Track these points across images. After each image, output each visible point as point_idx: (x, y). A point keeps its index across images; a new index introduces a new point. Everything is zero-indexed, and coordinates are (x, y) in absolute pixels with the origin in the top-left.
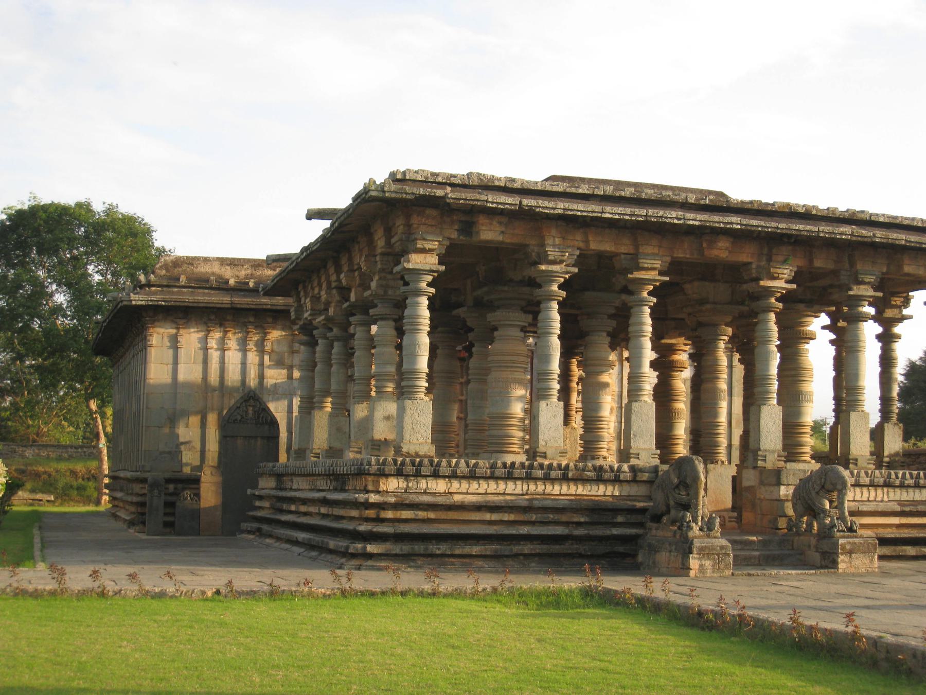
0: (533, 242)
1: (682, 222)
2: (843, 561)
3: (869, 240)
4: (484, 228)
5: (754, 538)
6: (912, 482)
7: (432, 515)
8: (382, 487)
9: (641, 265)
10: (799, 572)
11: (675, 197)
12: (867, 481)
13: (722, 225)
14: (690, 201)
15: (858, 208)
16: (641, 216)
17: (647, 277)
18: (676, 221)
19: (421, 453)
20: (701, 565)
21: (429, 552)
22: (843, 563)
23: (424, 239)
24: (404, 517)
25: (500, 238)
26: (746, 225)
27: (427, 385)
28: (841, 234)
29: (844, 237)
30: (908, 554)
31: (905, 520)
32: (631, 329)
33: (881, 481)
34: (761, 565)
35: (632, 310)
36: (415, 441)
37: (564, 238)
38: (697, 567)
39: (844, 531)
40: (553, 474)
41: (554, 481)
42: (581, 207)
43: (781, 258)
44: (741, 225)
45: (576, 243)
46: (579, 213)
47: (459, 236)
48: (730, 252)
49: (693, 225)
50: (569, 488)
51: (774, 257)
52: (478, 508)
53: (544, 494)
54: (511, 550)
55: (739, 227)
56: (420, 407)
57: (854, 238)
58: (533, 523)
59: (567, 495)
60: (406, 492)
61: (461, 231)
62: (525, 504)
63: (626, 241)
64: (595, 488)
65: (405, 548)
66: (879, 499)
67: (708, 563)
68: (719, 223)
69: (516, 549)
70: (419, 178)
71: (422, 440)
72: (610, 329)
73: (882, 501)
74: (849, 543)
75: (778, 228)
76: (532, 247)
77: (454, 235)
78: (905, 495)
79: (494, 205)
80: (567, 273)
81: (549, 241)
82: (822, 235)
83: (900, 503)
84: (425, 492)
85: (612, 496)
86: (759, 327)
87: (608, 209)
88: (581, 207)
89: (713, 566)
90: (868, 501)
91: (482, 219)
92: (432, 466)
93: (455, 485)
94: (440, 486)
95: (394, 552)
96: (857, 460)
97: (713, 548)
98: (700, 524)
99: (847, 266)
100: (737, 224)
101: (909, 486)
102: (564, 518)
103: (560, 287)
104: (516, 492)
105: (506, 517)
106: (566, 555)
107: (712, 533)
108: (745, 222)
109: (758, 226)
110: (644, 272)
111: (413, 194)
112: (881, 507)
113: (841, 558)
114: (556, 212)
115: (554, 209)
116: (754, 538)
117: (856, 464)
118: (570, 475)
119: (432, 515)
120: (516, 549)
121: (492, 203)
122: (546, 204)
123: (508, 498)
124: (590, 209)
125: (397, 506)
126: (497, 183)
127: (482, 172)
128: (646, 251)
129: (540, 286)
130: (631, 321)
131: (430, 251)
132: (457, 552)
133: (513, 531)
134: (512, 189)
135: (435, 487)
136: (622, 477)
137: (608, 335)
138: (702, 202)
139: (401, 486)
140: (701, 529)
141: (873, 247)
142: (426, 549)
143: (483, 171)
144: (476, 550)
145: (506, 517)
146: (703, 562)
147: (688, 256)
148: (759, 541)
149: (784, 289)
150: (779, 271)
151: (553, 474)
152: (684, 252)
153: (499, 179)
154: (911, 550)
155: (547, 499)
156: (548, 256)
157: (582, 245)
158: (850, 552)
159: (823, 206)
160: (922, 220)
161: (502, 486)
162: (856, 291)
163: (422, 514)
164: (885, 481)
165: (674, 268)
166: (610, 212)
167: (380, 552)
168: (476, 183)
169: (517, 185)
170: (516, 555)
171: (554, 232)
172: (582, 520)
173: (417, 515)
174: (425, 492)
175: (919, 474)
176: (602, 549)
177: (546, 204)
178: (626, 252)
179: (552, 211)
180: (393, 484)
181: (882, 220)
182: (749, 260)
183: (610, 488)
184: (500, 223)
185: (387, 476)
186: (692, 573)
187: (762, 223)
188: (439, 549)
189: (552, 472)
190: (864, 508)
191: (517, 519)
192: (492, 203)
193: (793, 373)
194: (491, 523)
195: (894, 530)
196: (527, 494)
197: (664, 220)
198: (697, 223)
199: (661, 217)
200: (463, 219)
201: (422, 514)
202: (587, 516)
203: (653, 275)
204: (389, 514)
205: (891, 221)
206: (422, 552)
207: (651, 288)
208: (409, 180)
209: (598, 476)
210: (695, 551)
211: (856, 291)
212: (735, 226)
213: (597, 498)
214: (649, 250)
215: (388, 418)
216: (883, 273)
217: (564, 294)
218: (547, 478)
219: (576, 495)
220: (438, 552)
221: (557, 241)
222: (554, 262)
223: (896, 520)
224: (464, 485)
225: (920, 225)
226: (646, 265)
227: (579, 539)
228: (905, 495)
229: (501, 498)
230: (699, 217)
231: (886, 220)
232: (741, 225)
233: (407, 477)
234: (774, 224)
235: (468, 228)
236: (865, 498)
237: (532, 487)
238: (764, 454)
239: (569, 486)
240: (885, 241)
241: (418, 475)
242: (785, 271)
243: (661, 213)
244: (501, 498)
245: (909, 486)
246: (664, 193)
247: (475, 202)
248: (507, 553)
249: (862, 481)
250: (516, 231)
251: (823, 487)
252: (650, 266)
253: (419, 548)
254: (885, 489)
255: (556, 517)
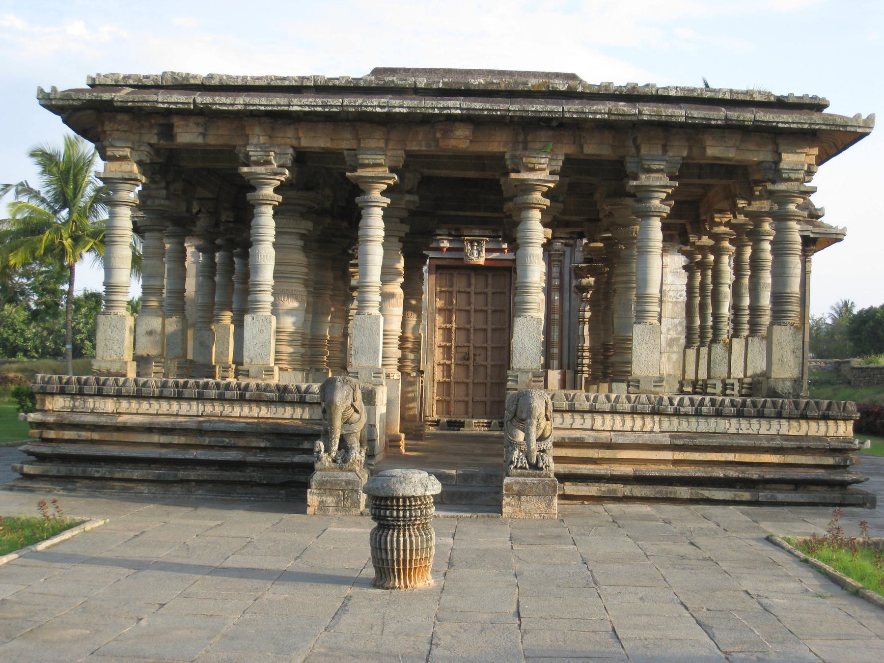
0: (239, 142)
1: (386, 110)
2: (509, 504)
3: (634, 118)
4: (179, 130)
5: (454, 472)
6: (690, 409)
7: (96, 436)
8: (49, 406)
9: (361, 161)
10: (449, 514)
11: (400, 82)
12: (627, 407)
13: (437, 111)
14: (419, 85)
15: (742, 87)
16: (336, 106)
17: (369, 174)
18: (379, 110)
19: (112, 371)
20: (321, 502)
21: (88, 475)
22: (509, 505)
23: (113, 146)
24: (66, 437)
25: (200, 140)
26: (468, 109)
27: (272, 299)
28: (595, 113)
29: (598, 116)
30: (678, 496)
31: (679, 456)
32: (360, 233)
33: (648, 408)
34: (444, 503)
35: (363, 212)
36: (108, 358)
37: (270, 137)
38: (316, 503)
39: (525, 468)
40: (228, 394)
41: (231, 401)
42: (264, 101)
43: (538, 145)
44: (461, 109)
45: (288, 141)
46: (263, 108)
47: (159, 140)
48: (471, 141)
49: (400, 113)
50: (251, 410)
51: (530, 145)
52: (149, 429)
53: (221, 416)
54: (176, 475)
55: (459, 112)
56: (113, 323)
57: (613, 118)
58: (210, 447)
59: (247, 417)
60: (72, 411)
61: (160, 135)
62: (193, 426)
63: (348, 135)
64: (280, 410)
65: (63, 469)
66: (648, 429)
67: (330, 500)
68: (433, 108)
69: (181, 474)
70: (109, 82)
71: (115, 357)
72: (403, 235)
73: (652, 432)
74: (519, 483)
75: (509, 111)
76: (238, 148)
77: (154, 140)
78: (684, 425)
79: (166, 106)
80: (670, 187)
81: (253, 140)
82: (567, 115)
83: (674, 435)
84: (92, 412)
85: (301, 419)
86: (520, 227)
87: (295, 101)
88: (264, 101)
89: (337, 503)
90: (632, 431)
91: (176, 121)
92: (98, 384)
93: (124, 405)
94: (109, 405)
95: (51, 474)
96: (639, 382)
97: (337, 483)
98: (333, 454)
99: (633, 150)
100: (457, 108)
101: (686, 415)
102: (241, 442)
103: (277, 190)
104: (151, 412)
105: (176, 440)
106: (243, 483)
107: (346, 466)
108: (465, 105)
109: (483, 110)
110: (370, 169)
111: (79, 99)
112: (646, 438)
113: (506, 500)
114: (235, 108)
115: (233, 105)
116: (454, 472)
117: (638, 387)
118: (248, 395)
119: (96, 436)
120: (181, 474)
121: (163, 103)
122: (224, 100)
123: (180, 419)
124: (274, 102)
125: (61, 426)
126: (192, 82)
127: (176, 71)
128: (369, 145)
129: (253, 189)
130: (361, 224)
131: (544, 170)
132: (117, 476)
133: (179, 455)
134: (210, 86)
135: (103, 406)
136: (308, 399)
137: (400, 241)
138: (434, 86)
139: (67, 404)
140: (334, 461)
141: (665, 127)
142: (84, 471)
143: (177, 70)
144: (136, 474)
145: (176, 440)
146: (324, 498)
147: (423, 148)
148: (458, 475)
149: (670, 187)
150: (534, 160)
151: (228, 394)
152: (419, 144)
153: (195, 77)
154: (684, 492)
155: (222, 421)
156: (782, 173)
157: (294, 142)
158: (519, 494)
159: (798, 93)
160: (731, 91)
161: (175, 406)
162: (645, 180)
163: (85, 435)
164: (653, 408)
165: (572, 168)
166: (297, 104)
167: (37, 473)
168: (169, 83)
169: (215, 82)
170: (182, 481)
171: (257, 130)
172: (262, 445)
173: (80, 436)
174: (92, 412)
175: (703, 400)
176: (280, 476)
177: (224, 100)
178: (347, 147)
179: (231, 108)
180: (58, 403)
181: (673, 93)
182: (502, 149)
183: (299, 411)
184: (197, 124)
185: (52, 394)
186: (310, 510)
187: (488, 106)
188: (98, 472)
189: (226, 392)
190: (620, 440)
191: (188, 442)
192: (163, 103)
193: (624, 278)
194: (163, 445)
195: (671, 467)
196: (202, 416)
197: (364, 109)
198: (405, 110)
199: (360, 106)
200: (161, 121)
201: (85, 435)
202: (269, 440)
203: (543, 175)
204: (52, 434)
205: (686, 94)
206: (80, 475)
207: (385, 187)
208: (100, 85)
209: (280, 397)
210: (313, 485)
211: (645, 180)
212: (453, 111)
213: (283, 422)
214: (373, 144)
215: (150, 333)
216: (683, 158)
217: (548, 202)
218: (221, 399)
219: (258, 418)
220: (97, 475)
221: (262, 140)
222: (258, 163)
223: (668, 455)
224: (134, 405)
225: (728, 97)
226: (367, 162)
227: (253, 464)
228: (684, 425)
229: (172, 419)
230: (407, 103)
231: (679, 94)
232: (461, 109)
233: (72, 395)
234: (503, 106)
235: (167, 132)
236: (648, 428)
237: (209, 408)
238: (515, 374)
239: (250, 408)
240: (656, 118)
241: (81, 393)
242: (543, 161)
243: (359, 101)
244: (172, 419)
245: (686, 415)
246: (387, 79)
247: (145, 104)
248: (171, 479)
249: (619, 407)
250: (220, 132)
251: (515, 415)
252: (371, 162)
253: (77, 470)
254: (657, 418)
255: (232, 441)
